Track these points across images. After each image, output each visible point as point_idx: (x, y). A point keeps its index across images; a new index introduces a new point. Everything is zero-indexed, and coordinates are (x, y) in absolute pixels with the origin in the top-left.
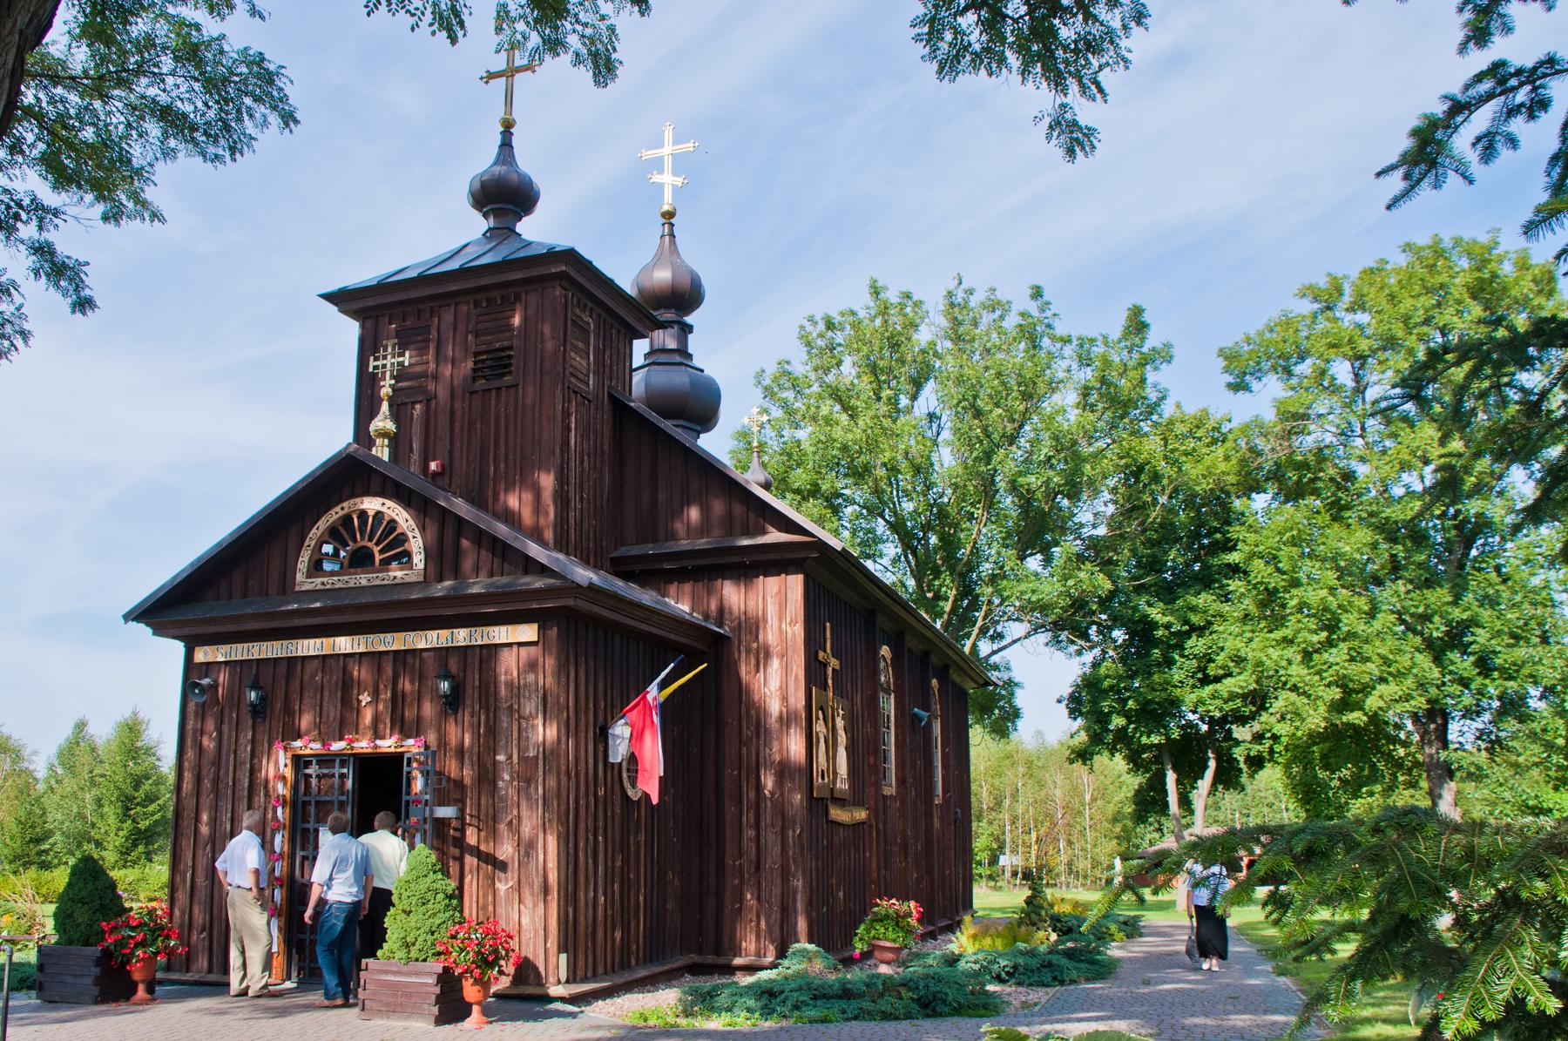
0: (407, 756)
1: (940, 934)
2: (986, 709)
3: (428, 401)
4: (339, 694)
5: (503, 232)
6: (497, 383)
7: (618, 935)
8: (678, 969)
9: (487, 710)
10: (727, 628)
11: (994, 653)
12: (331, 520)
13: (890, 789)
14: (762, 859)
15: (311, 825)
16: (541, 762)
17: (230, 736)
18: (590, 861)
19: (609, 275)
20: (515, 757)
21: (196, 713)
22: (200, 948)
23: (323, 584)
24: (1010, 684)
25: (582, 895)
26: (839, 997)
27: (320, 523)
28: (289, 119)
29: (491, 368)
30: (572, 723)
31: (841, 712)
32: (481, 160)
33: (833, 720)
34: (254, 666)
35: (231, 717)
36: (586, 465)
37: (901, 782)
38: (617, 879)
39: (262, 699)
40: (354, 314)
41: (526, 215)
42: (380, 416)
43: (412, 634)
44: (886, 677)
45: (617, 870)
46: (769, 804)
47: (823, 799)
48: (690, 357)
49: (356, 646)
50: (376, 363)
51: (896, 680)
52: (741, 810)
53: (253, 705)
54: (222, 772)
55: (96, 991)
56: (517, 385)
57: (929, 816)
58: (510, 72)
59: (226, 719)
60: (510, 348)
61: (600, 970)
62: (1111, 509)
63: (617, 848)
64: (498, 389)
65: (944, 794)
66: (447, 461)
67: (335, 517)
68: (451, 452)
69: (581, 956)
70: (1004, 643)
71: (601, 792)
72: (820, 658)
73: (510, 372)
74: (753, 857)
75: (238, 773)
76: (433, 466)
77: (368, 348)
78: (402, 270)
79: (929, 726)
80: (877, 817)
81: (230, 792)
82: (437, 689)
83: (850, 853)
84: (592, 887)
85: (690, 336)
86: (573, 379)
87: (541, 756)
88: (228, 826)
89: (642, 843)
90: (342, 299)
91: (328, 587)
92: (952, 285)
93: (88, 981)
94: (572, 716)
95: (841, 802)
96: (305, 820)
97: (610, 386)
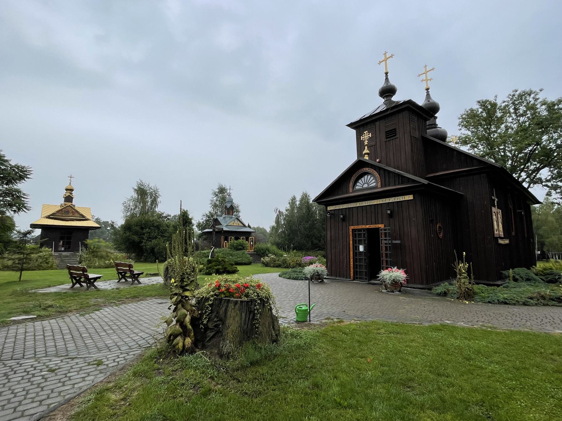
0: (380, 228)
15: (357, 245)
32: (381, 84)
40: (354, 128)
43: (379, 200)
48: (437, 125)
53: (342, 218)
58: (385, 60)
77: (359, 135)
78: (364, 116)
90: (351, 125)
95: (501, 238)
96: (356, 244)
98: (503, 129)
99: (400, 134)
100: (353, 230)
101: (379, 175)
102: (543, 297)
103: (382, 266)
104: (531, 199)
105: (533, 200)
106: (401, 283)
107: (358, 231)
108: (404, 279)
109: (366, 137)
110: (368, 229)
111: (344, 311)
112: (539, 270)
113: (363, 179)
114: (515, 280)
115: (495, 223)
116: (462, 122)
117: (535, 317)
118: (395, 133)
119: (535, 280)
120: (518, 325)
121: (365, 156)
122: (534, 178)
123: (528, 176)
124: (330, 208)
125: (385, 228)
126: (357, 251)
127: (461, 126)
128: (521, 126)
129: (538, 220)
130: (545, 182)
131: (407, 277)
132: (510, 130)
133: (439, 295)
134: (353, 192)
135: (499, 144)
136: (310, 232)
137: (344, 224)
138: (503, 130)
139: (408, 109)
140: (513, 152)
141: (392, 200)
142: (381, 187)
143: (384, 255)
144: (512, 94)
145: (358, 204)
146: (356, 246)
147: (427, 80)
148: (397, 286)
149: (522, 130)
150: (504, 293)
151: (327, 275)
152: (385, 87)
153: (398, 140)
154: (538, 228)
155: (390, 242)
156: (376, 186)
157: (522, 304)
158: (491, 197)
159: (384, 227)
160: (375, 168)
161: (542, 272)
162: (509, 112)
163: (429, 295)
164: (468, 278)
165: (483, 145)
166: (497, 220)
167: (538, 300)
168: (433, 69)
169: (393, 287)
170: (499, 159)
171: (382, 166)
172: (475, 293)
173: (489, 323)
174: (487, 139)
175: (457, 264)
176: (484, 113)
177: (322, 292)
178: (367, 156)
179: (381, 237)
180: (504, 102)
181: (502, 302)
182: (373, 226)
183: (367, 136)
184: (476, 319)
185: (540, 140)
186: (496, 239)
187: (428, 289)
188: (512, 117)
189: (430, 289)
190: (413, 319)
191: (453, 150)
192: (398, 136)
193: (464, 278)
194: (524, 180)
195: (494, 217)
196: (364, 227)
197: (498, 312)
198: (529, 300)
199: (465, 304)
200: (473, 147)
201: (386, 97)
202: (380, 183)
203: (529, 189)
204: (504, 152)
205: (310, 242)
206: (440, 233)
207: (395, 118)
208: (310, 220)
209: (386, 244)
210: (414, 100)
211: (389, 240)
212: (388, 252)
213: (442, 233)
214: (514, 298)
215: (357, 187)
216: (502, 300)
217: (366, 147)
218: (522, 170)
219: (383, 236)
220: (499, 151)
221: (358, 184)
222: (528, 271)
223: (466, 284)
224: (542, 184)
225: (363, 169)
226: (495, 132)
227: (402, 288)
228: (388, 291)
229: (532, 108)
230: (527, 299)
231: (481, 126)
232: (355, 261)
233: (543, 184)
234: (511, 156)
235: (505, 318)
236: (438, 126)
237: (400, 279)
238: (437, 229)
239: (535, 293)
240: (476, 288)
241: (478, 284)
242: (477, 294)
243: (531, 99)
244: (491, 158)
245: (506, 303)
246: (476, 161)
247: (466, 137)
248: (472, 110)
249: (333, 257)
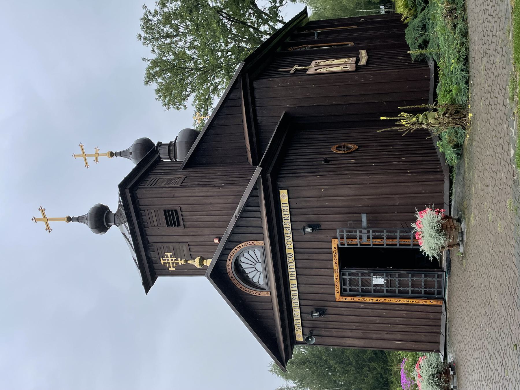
0: (340, 246)
5: (116, 219)
15: (372, 288)
19: (131, 170)
32: (85, 228)
39: (317, 310)
40: (154, 280)
42: (194, 264)
48: (171, 142)
50: (172, 267)
53: (320, 315)
58: (46, 220)
64: (182, 216)
66: (215, 236)
77: (166, 273)
85: (163, 143)
90: (147, 285)
95: (358, 61)
98: (193, 51)
99: (172, 204)
100: (342, 295)
101: (241, 242)
102: (452, 11)
103: (411, 247)
104: (298, 20)
105: (301, 18)
106: (442, 219)
107: (344, 284)
108: (434, 213)
109: (170, 262)
110: (341, 267)
111: (516, 345)
112: (408, 13)
113: (247, 271)
114: (425, 44)
115: (333, 69)
116: (175, 105)
117: (486, 24)
118: (172, 211)
119: (424, 19)
120: (504, 48)
121: (205, 264)
122: (269, 16)
123: (265, 22)
124: (299, 336)
125: (339, 237)
126: (385, 289)
127: (180, 107)
128: (190, 30)
129: (333, 9)
130: (276, 3)
131: (431, 208)
132: (196, 44)
133: (460, 156)
134: (269, 290)
135: (214, 58)
136: (350, 364)
137: (330, 310)
138: (195, 52)
139: (132, 191)
140: (228, 40)
141: (287, 223)
142: (263, 240)
143: (390, 242)
144: (143, 41)
145: (293, 282)
146: (375, 291)
147: (97, 155)
148: (449, 226)
149: (197, 30)
150: (449, 62)
151: (438, 351)
152: (91, 224)
153: (184, 207)
154: (345, 9)
155: (365, 231)
156: (261, 249)
157: (466, 39)
158: (292, 74)
159: (337, 238)
160: (226, 254)
161: (410, 9)
162: (170, 44)
163: (462, 171)
164: (427, 112)
165: (214, 77)
166: (328, 67)
167: (456, 17)
168: (82, 146)
169: (452, 232)
170: (237, 58)
171: (225, 238)
172: (453, 102)
173: (505, 89)
174: (205, 72)
175: (402, 128)
176: (166, 76)
177: (476, 376)
178: (205, 261)
180: (153, 51)
181: (464, 65)
182: (335, 258)
183: (170, 258)
184: (501, 106)
185: (214, 10)
186: (359, 68)
187: (451, 172)
188: (176, 41)
189: (451, 168)
190: (515, 211)
191: (212, 125)
192: (177, 208)
193: (427, 119)
194: (272, 28)
195: (323, 70)
196: (336, 274)
197: (483, 73)
198: (458, 28)
199: (473, 118)
200: (216, 89)
201: (108, 221)
202: (255, 242)
203: (287, 20)
204: (228, 51)
205: (372, 364)
206: (348, 148)
207: (146, 211)
208: (326, 360)
209: (369, 238)
210: (121, 179)
211: (361, 232)
212: (385, 234)
213: (349, 145)
214: (456, 49)
215: (262, 282)
216: (460, 66)
217: (189, 262)
218: (256, 30)
219: (353, 241)
220: (226, 57)
221: (255, 280)
222: (411, 26)
223: (437, 116)
224: (278, 7)
225: (228, 270)
226: (195, 63)
227: (452, 215)
228: (462, 241)
229: (167, 19)
230: (457, 33)
231: (184, 80)
232: (403, 294)
233: (278, 4)
234: (233, 43)
235: (494, 65)
236: (173, 140)
237: (436, 220)
238: (342, 152)
239: (445, 21)
240: (443, 100)
241: (435, 95)
242: (455, 100)
243: (155, 19)
244: (234, 68)
245: (467, 60)
246: (232, 94)
247: (200, 100)
248: (158, 91)
249: (399, 336)
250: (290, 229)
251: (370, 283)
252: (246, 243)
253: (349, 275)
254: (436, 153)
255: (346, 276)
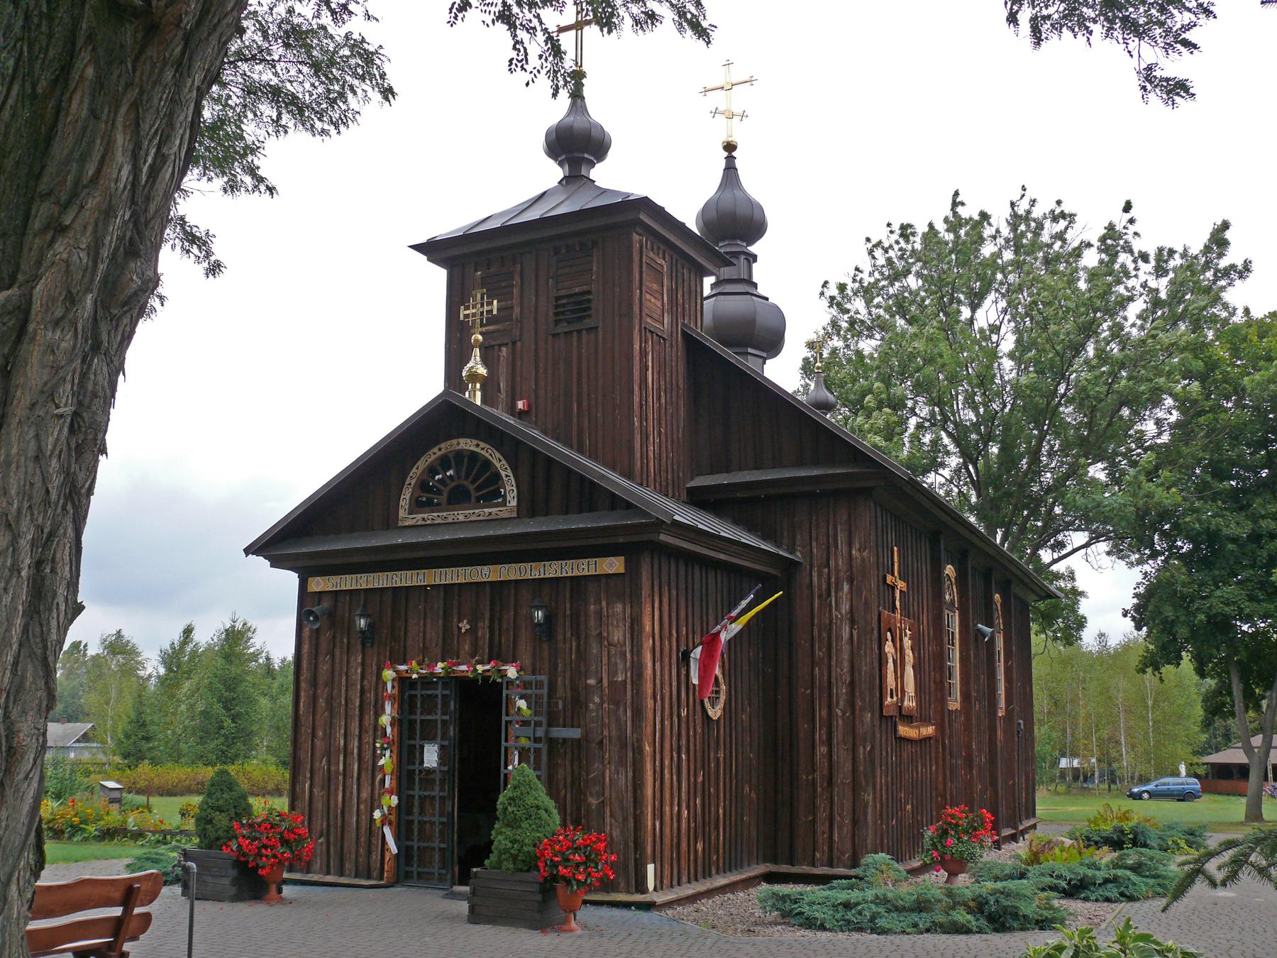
1: (1004, 843)
2: (1047, 619)
3: (514, 343)
4: (441, 622)
5: (575, 178)
6: (578, 326)
7: (700, 846)
8: (755, 877)
9: (578, 638)
10: (798, 554)
11: (1055, 561)
12: (430, 460)
13: (954, 704)
14: (835, 773)
15: (417, 742)
16: (629, 686)
17: (341, 660)
18: (675, 777)
20: (605, 681)
21: (310, 637)
22: (318, 851)
23: (424, 519)
24: (1076, 594)
25: (667, 809)
26: (912, 910)
27: (419, 463)
28: (388, 93)
29: (573, 312)
30: (658, 649)
31: (908, 632)
33: (901, 640)
34: (362, 597)
35: (342, 642)
36: (663, 401)
37: (966, 696)
38: (699, 794)
41: (598, 162)
43: (507, 566)
44: (951, 595)
45: (699, 786)
46: (840, 722)
47: (891, 717)
48: (755, 285)
49: (455, 577)
51: (960, 597)
52: (814, 727)
53: (362, 632)
54: (335, 692)
55: (233, 891)
56: (597, 328)
57: (992, 729)
59: (338, 645)
60: (589, 292)
61: (684, 879)
62: (1175, 416)
63: (699, 765)
64: (579, 331)
65: (1007, 708)
67: (433, 457)
68: (536, 391)
69: (667, 867)
70: (1064, 552)
71: (684, 713)
72: (888, 581)
73: (589, 316)
74: (825, 772)
75: (350, 693)
76: (520, 405)
77: (456, 298)
79: (992, 640)
80: (943, 733)
81: (342, 711)
82: (532, 617)
83: (917, 767)
84: (676, 802)
86: (649, 320)
87: (629, 681)
88: (342, 742)
89: (721, 759)
90: (432, 249)
91: (429, 522)
92: (1015, 198)
93: (226, 881)
94: (658, 644)
95: (908, 718)
96: (411, 737)
97: (683, 324)
179: (506, 741)
186: (889, 721)
217: (477, 351)
250: (542, 576)
251: (430, 738)
252: (514, 483)
253: (443, 696)
254: (710, 876)
255: (443, 689)
